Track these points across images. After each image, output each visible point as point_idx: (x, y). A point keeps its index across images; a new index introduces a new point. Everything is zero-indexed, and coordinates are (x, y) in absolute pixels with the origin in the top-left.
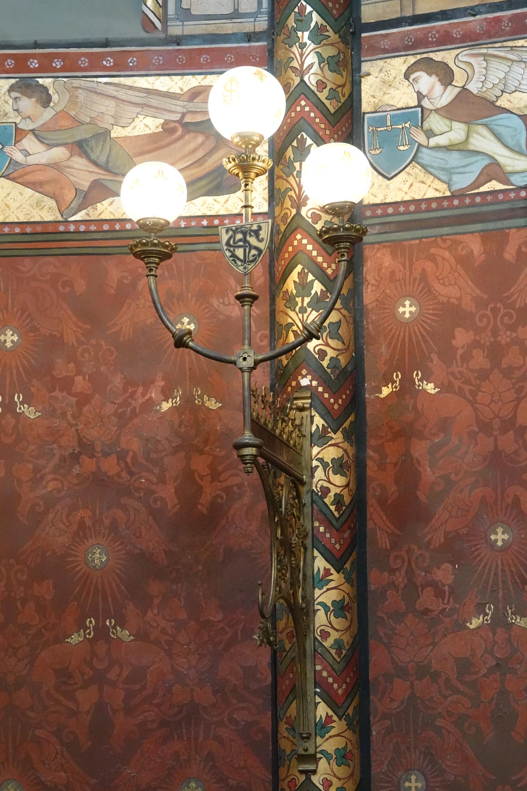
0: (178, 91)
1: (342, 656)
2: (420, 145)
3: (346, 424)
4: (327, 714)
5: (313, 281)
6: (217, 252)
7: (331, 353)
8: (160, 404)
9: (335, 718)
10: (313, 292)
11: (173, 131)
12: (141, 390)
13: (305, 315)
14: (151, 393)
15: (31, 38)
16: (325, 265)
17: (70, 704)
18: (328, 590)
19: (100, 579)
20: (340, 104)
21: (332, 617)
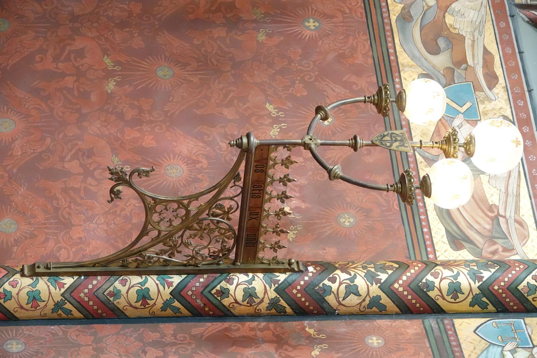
0: (521, 214)
1: (109, 297)
2: (503, 347)
3: (283, 302)
4: (66, 284)
5: (387, 273)
6: (405, 238)
7: (335, 286)
8: (288, 206)
9: (63, 290)
10: (379, 273)
11: (492, 211)
12: (297, 195)
13: (361, 269)
14: (295, 201)
15: (533, 85)
16: (401, 282)
17: (68, 157)
18: (157, 285)
19: (158, 173)
20: (526, 295)
21: (136, 288)
